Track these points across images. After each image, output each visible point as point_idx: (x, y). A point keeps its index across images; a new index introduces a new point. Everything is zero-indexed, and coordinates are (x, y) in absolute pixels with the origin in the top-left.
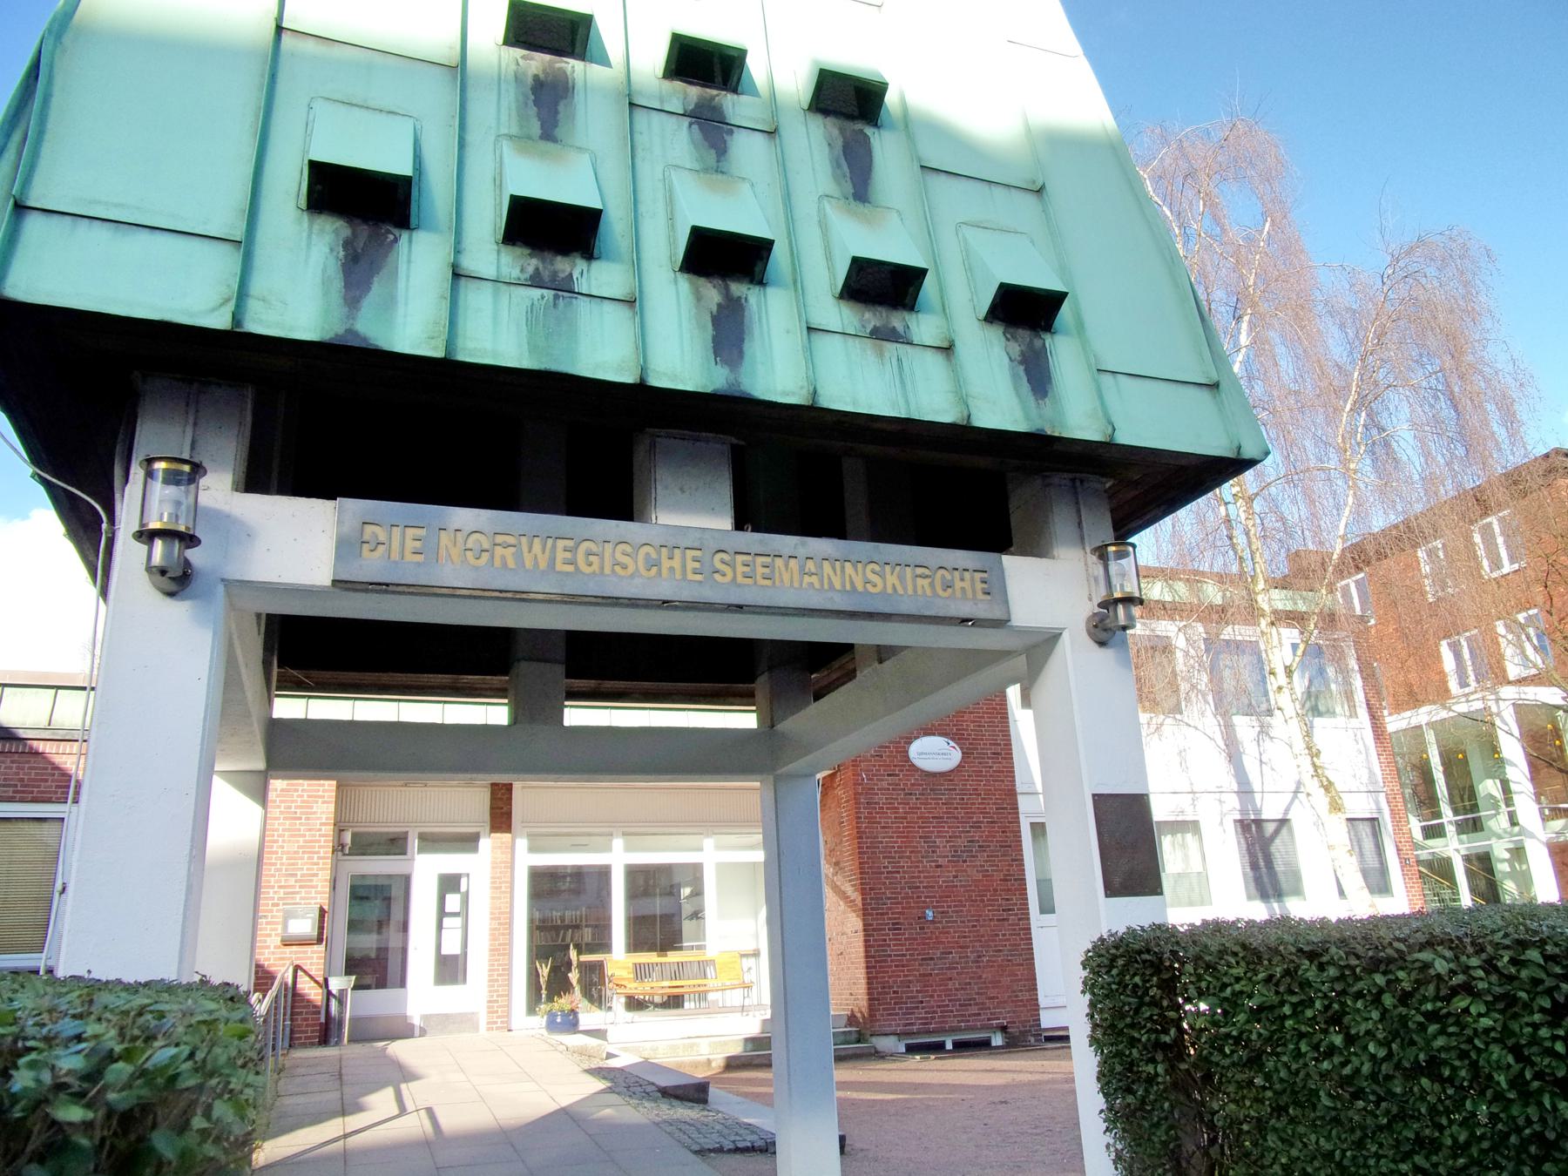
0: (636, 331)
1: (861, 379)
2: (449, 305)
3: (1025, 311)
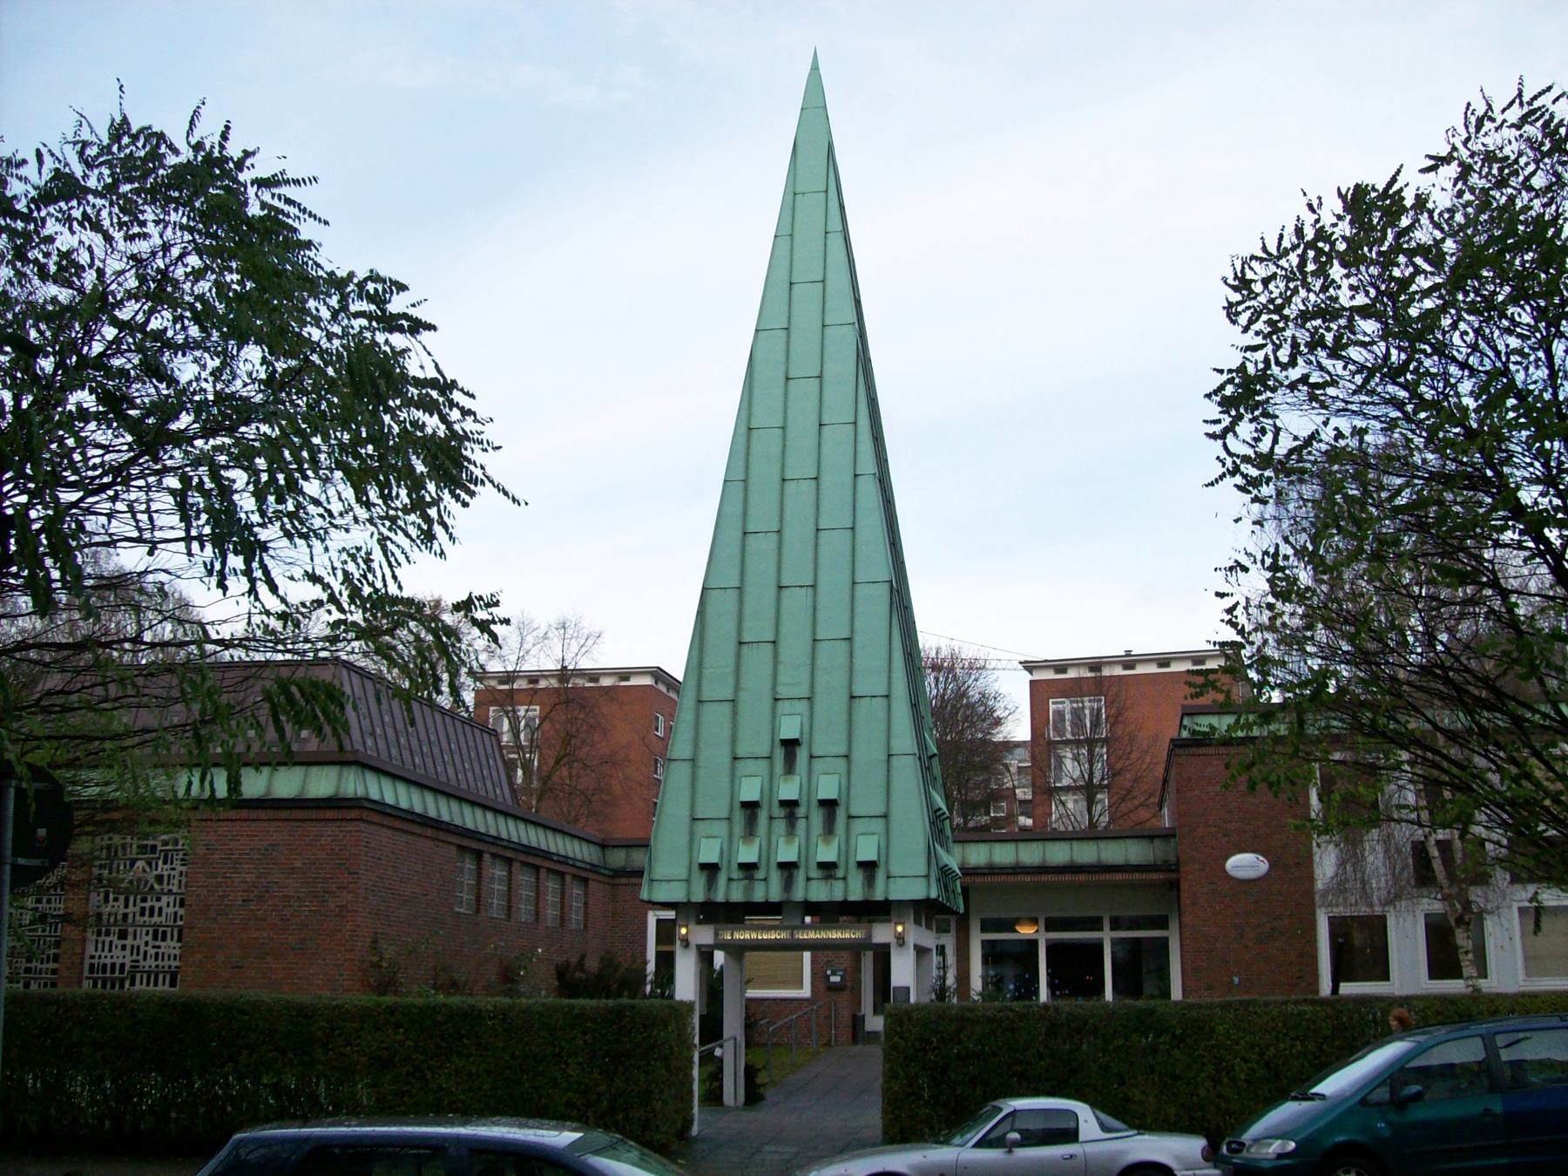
0: (770, 889)
1: (820, 892)
2: (730, 891)
3: (869, 867)
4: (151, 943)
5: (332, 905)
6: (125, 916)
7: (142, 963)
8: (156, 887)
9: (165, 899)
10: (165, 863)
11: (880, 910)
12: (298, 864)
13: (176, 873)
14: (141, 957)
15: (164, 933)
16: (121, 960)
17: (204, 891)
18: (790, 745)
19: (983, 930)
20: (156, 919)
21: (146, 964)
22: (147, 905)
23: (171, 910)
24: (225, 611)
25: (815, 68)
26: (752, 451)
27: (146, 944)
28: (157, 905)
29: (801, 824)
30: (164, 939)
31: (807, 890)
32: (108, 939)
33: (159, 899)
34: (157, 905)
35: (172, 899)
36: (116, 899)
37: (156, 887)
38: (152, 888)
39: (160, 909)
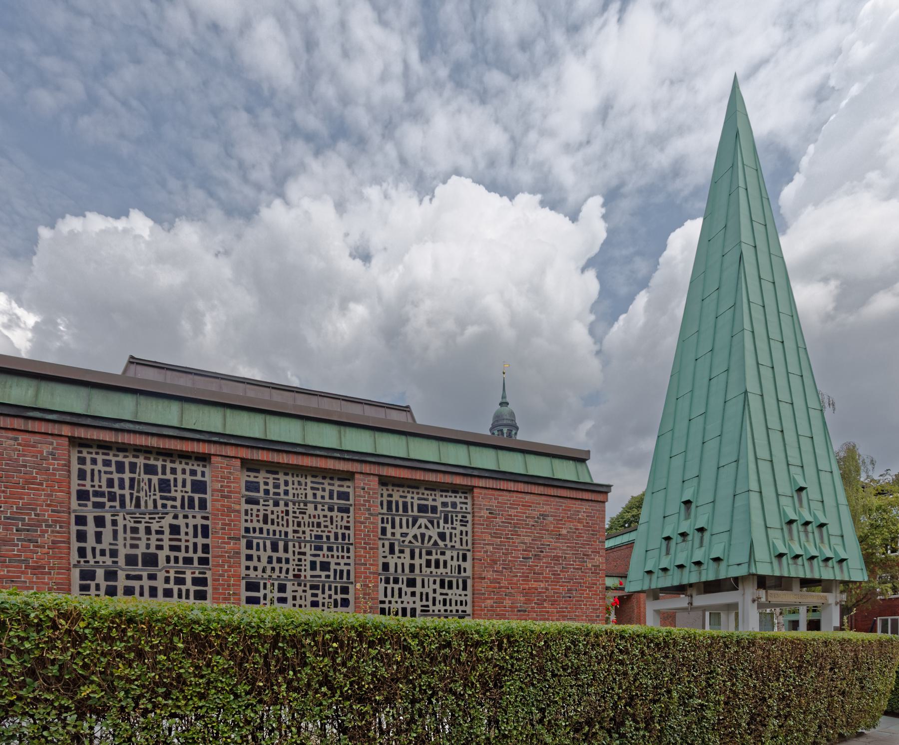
4: (439, 591)
5: (590, 565)
6: (412, 567)
7: (431, 608)
8: (439, 542)
9: (448, 553)
10: (446, 522)
11: (734, 584)
12: (564, 532)
13: (458, 532)
14: (430, 603)
15: (450, 583)
16: (412, 605)
17: (491, 548)
18: (688, 503)
19: (247, 590)
20: (441, 570)
21: (436, 608)
22: (433, 558)
23: (455, 563)
24: (289, 376)
25: (742, 253)
26: (206, 409)
27: (435, 591)
28: (442, 558)
29: (811, 535)
30: (450, 587)
31: (727, 571)
32: (396, 587)
33: (443, 553)
34: (442, 558)
35: (455, 554)
36: (401, 551)
37: (439, 542)
38: (436, 543)
39: (445, 562)
